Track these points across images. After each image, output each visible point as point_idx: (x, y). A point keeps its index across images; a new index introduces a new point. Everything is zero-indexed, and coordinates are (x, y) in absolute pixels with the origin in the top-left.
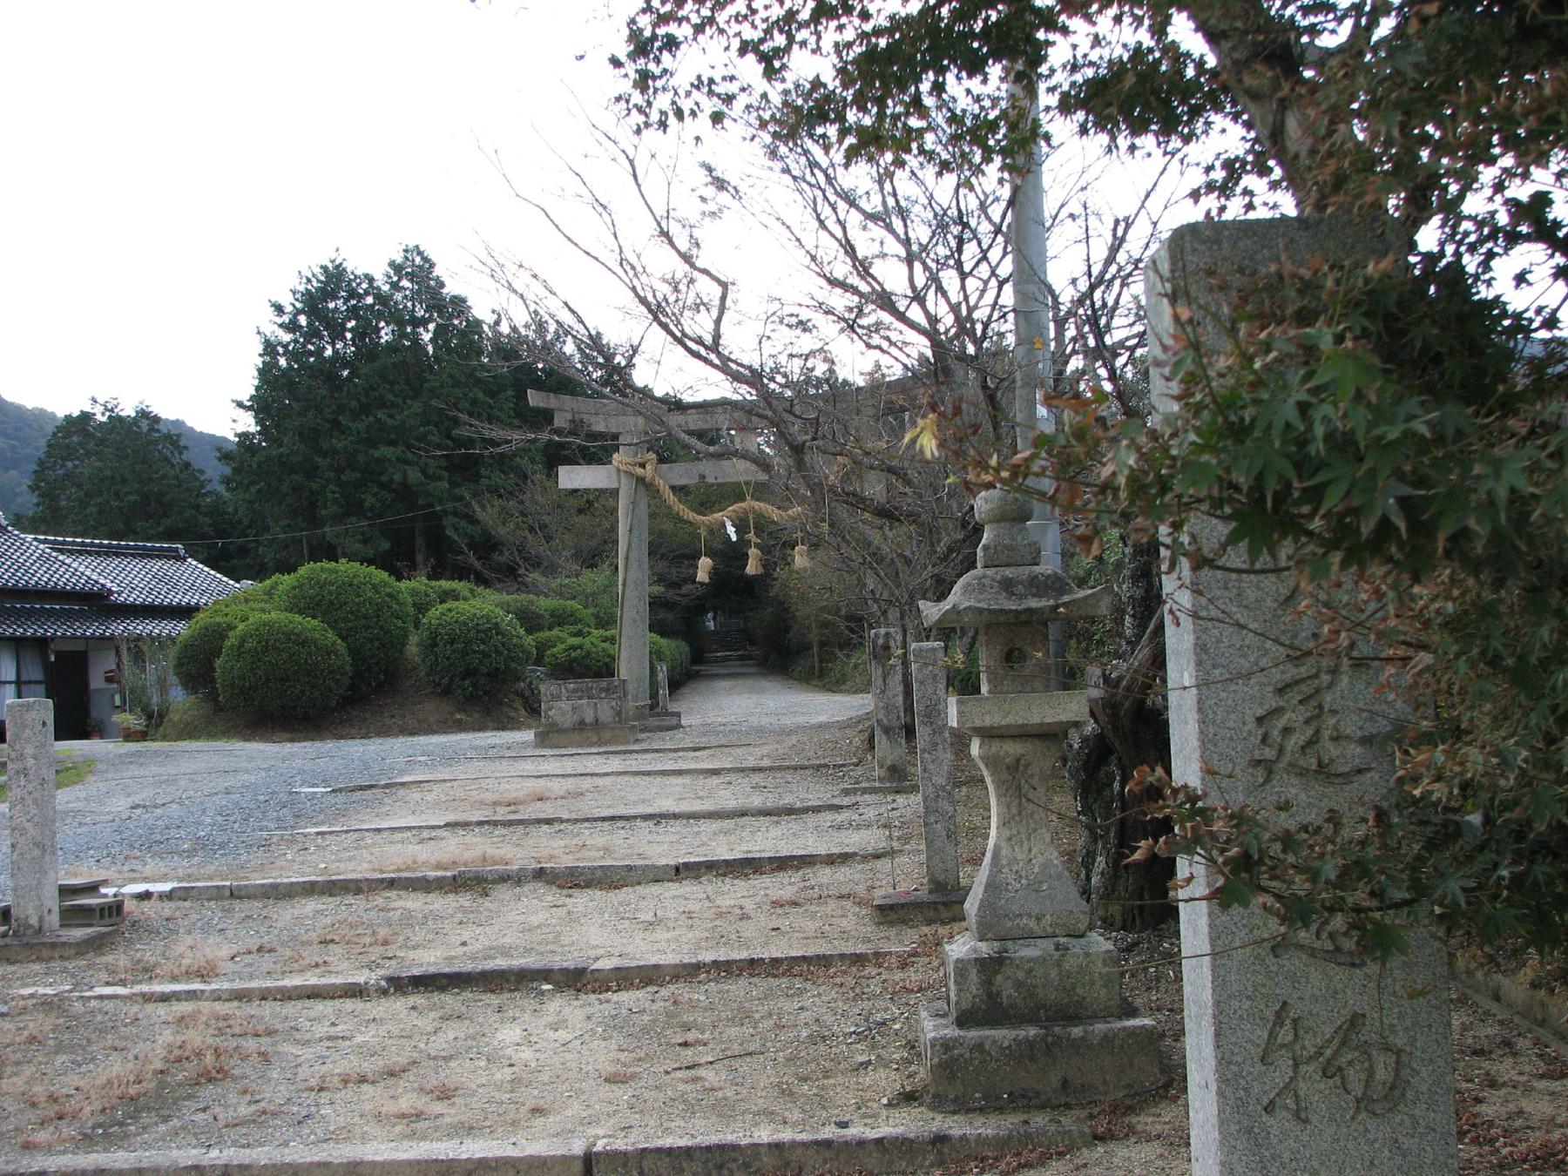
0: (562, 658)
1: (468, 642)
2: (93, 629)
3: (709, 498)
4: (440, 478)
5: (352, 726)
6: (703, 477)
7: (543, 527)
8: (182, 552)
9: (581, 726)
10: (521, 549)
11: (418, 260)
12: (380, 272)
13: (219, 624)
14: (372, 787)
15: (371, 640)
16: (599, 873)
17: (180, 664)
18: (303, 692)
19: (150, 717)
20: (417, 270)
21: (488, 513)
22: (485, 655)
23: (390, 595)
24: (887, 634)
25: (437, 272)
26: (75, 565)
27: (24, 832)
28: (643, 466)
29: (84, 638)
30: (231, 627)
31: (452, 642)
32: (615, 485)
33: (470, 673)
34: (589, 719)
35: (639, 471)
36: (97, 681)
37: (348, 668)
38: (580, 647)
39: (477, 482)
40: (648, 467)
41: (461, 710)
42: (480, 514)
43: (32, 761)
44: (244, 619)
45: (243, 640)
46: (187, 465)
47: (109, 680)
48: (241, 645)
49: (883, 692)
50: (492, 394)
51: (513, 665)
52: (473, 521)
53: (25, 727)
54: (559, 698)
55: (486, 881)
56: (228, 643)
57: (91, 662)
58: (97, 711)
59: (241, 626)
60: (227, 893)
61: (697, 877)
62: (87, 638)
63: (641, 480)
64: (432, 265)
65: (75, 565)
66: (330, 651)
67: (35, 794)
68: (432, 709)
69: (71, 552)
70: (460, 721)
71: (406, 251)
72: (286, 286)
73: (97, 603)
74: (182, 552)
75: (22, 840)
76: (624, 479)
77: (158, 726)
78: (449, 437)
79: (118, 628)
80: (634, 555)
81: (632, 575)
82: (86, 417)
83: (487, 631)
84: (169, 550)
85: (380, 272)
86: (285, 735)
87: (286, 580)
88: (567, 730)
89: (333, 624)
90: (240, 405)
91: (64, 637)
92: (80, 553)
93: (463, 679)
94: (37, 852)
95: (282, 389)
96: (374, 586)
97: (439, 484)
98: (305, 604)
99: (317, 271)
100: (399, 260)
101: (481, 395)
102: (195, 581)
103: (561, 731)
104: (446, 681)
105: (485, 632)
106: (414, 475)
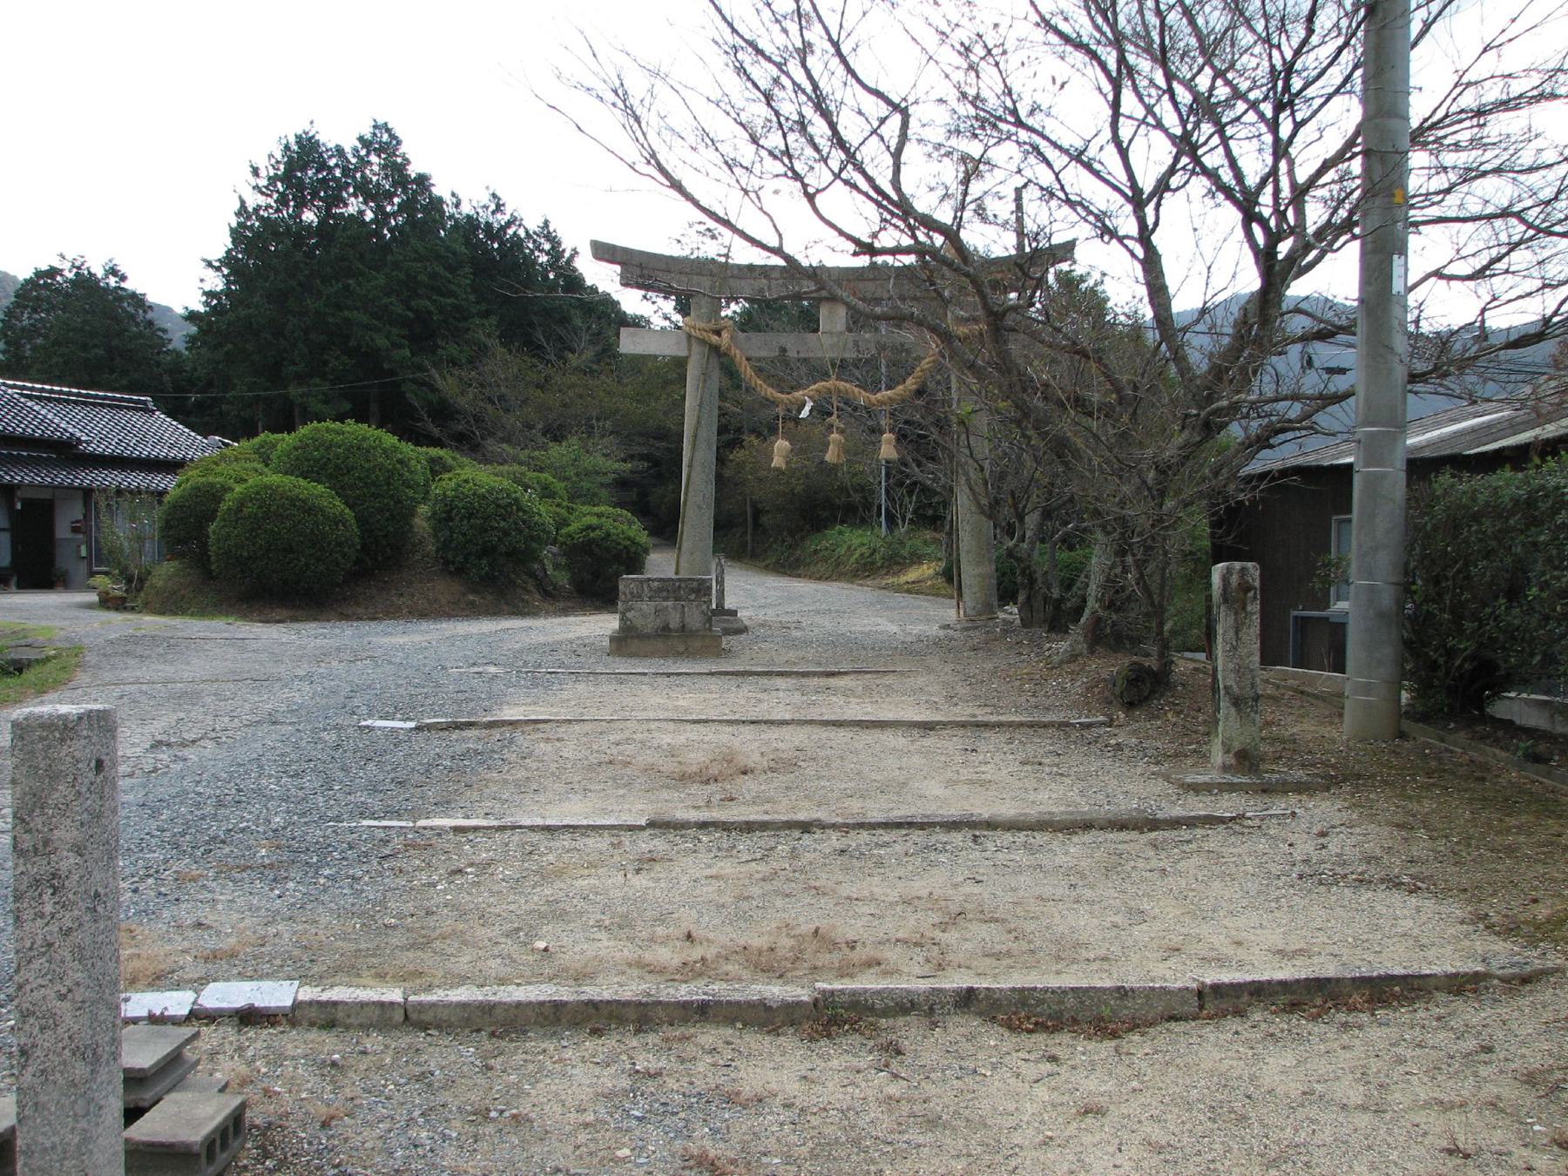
0: (579, 538)
1: (487, 518)
2: (63, 477)
3: (784, 371)
4: (400, 347)
5: (358, 604)
6: (783, 350)
7: (502, 398)
8: (151, 406)
9: (665, 631)
10: (478, 419)
11: (385, 137)
12: (349, 143)
13: (212, 485)
14: (470, 725)
15: (381, 510)
16: (1070, 1001)
17: (167, 526)
18: (307, 565)
19: (129, 581)
20: (383, 143)
21: (447, 384)
22: (506, 533)
23: (400, 462)
24: (1243, 569)
25: (402, 149)
26: (43, 412)
27: (50, 1022)
28: (718, 333)
29: (51, 487)
30: (226, 489)
31: (470, 516)
32: (684, 353)
33: (487, 551)
34: (674, 622)
35: (714, 339)
36: (62, 530)
37: (357, 540)
38: (600, 527)
39: (434, 353)
40: (725, 335)
41: (475, 591)
42: (440, 384)
43: (73, 859)
44: (242, 480)
45: (241, 504)
46: (150, 323)
47: (75, 530)
48: (239, 510)
49: (1235, 648)
50: (450, 268)
51: (534, 545)
52: (433, 389)
53: (55, 777)
54: (639, 597)
55: (871, 1009)
56: (223, 507)
57: (57, 511)
58: (64, 560)
59: (238, 489)
60: (398, 1016)
61: (1240, 1013)
62: (55, 487)
63: (715, 349)
64: (399, 143)
65: (43, 412)
66: (337, 521)
67: (77, 937)
68: (444, 588)
69: (40, 398)
70: (472, 603)
71: (375, 127)
72: (266, 147)
73: (66, 452)
74: (151, 406)
75: (46, 1041)
76: (696, 348)
77: (138, 590)
78: (409, 308)
79: (86, 478)
80: (703, 434)
81: (699, 455)
82: (53, 272)
83: (508, 508)
84: (139, 402)
85: (349, 143)
86: (285, 613)
87: (286, 440)
88: (648, 637)
89: (341, 490)
90: (210, 264)
91: (31, 485)
92: (49, 399)
93: (480, 558)
94: (80, 1070)
95: (260, 253)
96: (385, 451)
97: (401, 352)
98: (307, 465)
99: (292, 140)
100: (368, 136)
101: (440, 269)
102: (163, 434)
103: (643, 637)
104: (460, 558)
105: (505, 507)
106: (381, 342)
